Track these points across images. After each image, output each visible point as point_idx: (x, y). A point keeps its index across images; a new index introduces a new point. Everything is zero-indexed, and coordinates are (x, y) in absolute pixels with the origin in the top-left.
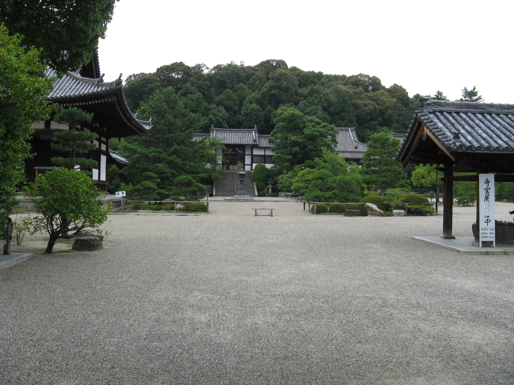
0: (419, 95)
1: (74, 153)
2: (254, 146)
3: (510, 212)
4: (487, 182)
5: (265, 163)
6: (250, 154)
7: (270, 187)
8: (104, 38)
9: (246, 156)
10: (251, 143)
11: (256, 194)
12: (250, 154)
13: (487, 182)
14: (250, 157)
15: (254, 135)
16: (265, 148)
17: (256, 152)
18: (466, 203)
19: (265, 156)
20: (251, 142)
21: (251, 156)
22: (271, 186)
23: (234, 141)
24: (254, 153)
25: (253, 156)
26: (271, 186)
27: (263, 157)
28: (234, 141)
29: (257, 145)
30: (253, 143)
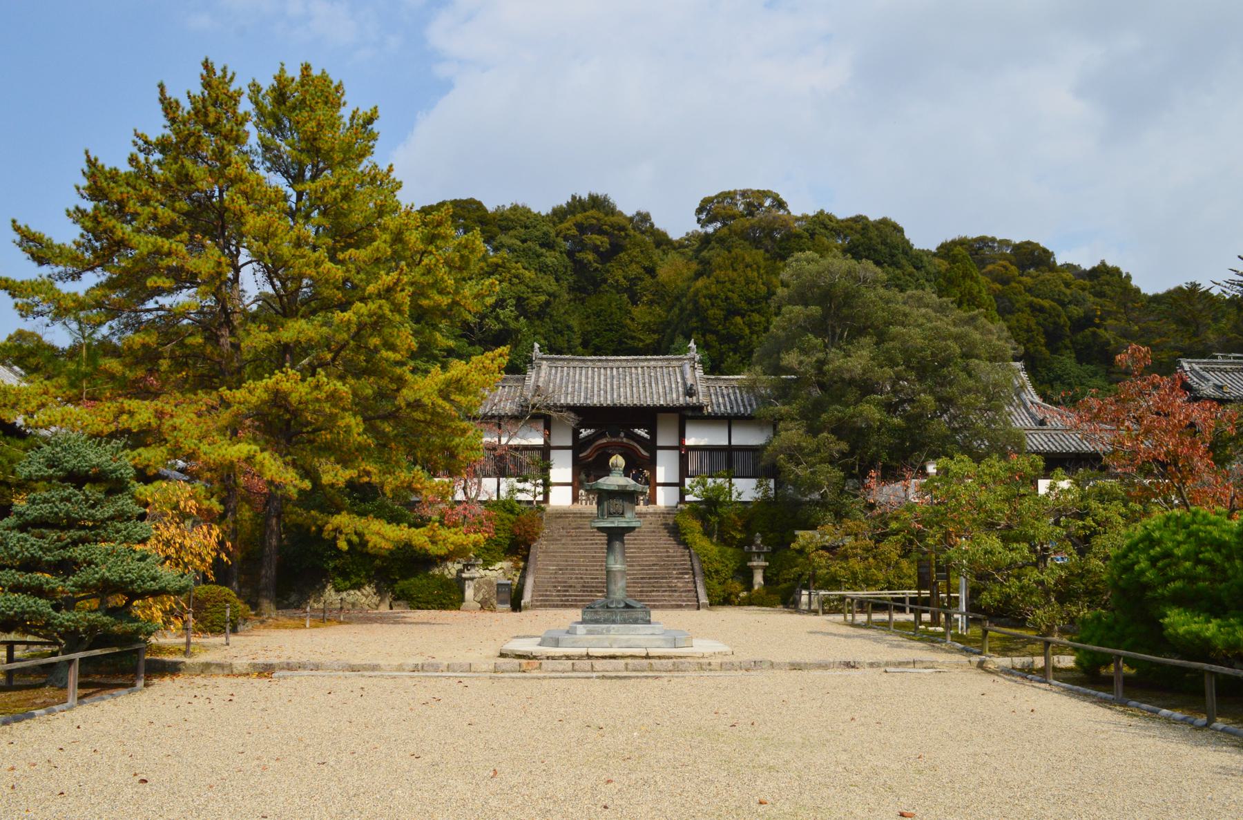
2: (688, 415)
3: (207, 61)
5: (731, 476)
6: (675, 443)
7: (757, 567)
8: (202, 75)
9: (659, 453)
10: (678, 399)
11: (704, 600)
17: (695, 437)
18: (1107, 665)
19: (729, 450)
20: (676, 398)
21: (677, 452)
22: (764, 564)
24: (690, 441)
25: (684, 453)
26: (764, 564)
27: (723, 456)
29: (700, 408)
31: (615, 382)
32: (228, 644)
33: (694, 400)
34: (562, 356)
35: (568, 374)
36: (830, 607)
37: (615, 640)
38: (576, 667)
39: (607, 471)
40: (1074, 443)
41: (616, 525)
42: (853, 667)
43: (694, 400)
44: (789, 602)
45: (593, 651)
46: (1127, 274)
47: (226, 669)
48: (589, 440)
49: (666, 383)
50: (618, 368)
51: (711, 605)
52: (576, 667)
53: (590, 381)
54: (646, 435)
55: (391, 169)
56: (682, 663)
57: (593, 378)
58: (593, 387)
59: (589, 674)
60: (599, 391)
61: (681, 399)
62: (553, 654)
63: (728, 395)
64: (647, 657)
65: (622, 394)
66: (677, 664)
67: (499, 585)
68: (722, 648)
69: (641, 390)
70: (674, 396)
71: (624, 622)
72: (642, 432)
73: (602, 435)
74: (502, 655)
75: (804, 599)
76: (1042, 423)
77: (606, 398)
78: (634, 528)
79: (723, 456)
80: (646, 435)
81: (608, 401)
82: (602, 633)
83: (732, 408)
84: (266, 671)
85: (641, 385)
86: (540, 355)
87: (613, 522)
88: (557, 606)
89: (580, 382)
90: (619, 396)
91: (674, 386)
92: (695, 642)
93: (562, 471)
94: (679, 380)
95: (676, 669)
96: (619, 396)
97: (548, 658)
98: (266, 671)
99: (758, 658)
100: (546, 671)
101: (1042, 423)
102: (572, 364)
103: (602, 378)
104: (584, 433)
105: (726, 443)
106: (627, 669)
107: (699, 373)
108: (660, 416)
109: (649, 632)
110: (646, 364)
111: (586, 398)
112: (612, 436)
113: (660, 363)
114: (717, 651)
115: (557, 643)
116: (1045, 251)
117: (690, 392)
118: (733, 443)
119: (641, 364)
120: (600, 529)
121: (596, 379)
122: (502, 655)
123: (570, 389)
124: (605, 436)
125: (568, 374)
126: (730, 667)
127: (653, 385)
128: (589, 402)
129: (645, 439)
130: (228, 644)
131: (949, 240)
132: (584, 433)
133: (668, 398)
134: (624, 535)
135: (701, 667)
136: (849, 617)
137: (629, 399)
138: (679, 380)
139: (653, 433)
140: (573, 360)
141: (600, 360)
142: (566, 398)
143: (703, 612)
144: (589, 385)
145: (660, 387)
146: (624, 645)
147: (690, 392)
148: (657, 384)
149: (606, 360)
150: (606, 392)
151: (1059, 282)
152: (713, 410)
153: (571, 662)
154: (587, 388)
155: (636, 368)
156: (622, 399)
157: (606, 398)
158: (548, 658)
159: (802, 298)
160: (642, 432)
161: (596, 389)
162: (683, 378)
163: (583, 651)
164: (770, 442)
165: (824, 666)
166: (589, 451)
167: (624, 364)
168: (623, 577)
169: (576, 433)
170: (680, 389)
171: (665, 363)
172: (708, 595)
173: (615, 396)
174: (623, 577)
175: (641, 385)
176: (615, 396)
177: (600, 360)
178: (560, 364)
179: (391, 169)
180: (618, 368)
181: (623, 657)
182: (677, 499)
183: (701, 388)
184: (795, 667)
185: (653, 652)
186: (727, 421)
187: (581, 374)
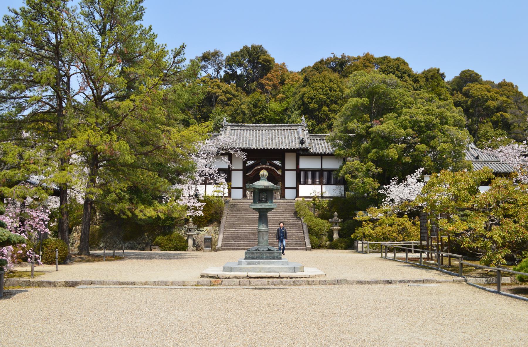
0: (359, 56)
1: (127, 210)
4: (33, 178)
7: (336, 229)
9: (286, 172)
10: (296, 145)
11: (309, 246)
12: (295, 168)
13: (33, 178)
14: (294, 174)
15: (303, 133)
16: (322, 156)
17: (305, 164)
21: (295, 172)
23: (263, 143)
28: (263, 143)
29: (307, 150)
30: (298, 146)
31: (264, 137)
32: (57, 270)
33: (304, 146)
34: (238, 124)
35: (240, 133)
36: (375, 249)
37: (263, 268)
38: (241, 283)
39: (258, 178)
40: (494, 168)
41: (263, 207)
42: (390, 283)
43: (304, 146)
44: (351, 246)
45: (251, 274)
46: (516, 86)
47: (52, 284)
48: (252, 166)
49: (290, 138)
50: (265, 130)
51: (312, 248)
52: (241, 283)
53: (251, 136)
54: (280, 165)
55: (150, 29)
56: (298, 281)
57: (253, 135)
58: (253, 140)
59: (248, 287)
60: (256, 142)
61: (297, 145)
62: (228, 276)
63: (321, 144)
64: (279, 277)
65: (267, 143)
66: (295, 281)
67: (205, 238)
68: (320, 272)
69: (277, 141)
70: (294, 144)
71: (267, 258)
72: (277, 163)
73: (258, 164)
74: (202, 276)
75: (360, 245)
76: (477, 158)
77: (259, 145)
78: (273, 209)
79: (318, 174)
80: (280, 165)
81: (260, 146)
82: (255, 264)
83: (323, 150)
84: (72, 284)
85: (277, 138)
86: (227, 123)
87: (261, 205)
88: (234, 249)
89: (246, 137)
90: (266, 144)
91: (293, 139)
92: (305, 269)
93: (238, 179)
94: (296, 136)
95: (295, 284)
96: (266, 144)
97: (226, 278)
98: (72, 284)
99: (339, 278)
100: (225, 285)
101: (477, 158)
102: (242, 128)
103: (258, 135)
104: (250, 163)
105: (319, 167)
106: (268, 284)
107: (306, 132)
108: (287, 154)
109: (281, 264)
110: (279, 128)
111: (249, 145)
112: (263, 164)
113: (287, 128)
114: (317, 274)
115: (231, 270)
116: (477, 74)
117: (302, 142)
118: (323, 168)
119: (277, 128)
120: (254, 209)
121: (254, 136)
122: (202, 276)
123: (241, 141)
124: (260, 165)
125: (240, 133)
126: (324, 283)
127: (283, 138)
128: (251, 147)
129: (279, 166)
130: (57, 270)
131: (426, 70)
132: (250, 163)
133: (291, 145)
134: (267, 212)
135: (308, 283)
136: (384, 255)
137: (271, 145)
138: (296, 136)
139: (283, 163)
140: (243, 126)
141: (256, 126)
142: (239, 145)
143: (308, 252)
144: (251, 139)
145: (287, 139)
146: (267, 271)
147: (302, 142)
148: (285, 138)
149: (260, 126)
150: (259, 142)
151: (484, 89)
152: (313, 151)
153: (238, 280)
154: (250, 140)
155: (275, 130)
156: (267, 145)
157: (259, 145)
158: (226, 278)
159: (359, 94)
160: (277, 163)
161: (254, 141)
162: (298, 135)
163: (245, 274)
164: (341, 167)
165: (376, 282)
166: (251, 172)
167: (269, 128)
168: (266, 235)
169: (244, 163)
170: (297, 140)
171: (289, 128)
172: (311, 243)
173: (264, 144)
174: (266, 235)
175: (277, 138)
176: (264, 144)
177: (256, 126)
178: (236, 128)
179: (150, 29)
180: (265, 130)
181: (266, 278)
182: (295, 195)
183: (307, 140)
184: (360, 282)
185: (283, 274)
186: (320, 157)
187: (247, 133)
